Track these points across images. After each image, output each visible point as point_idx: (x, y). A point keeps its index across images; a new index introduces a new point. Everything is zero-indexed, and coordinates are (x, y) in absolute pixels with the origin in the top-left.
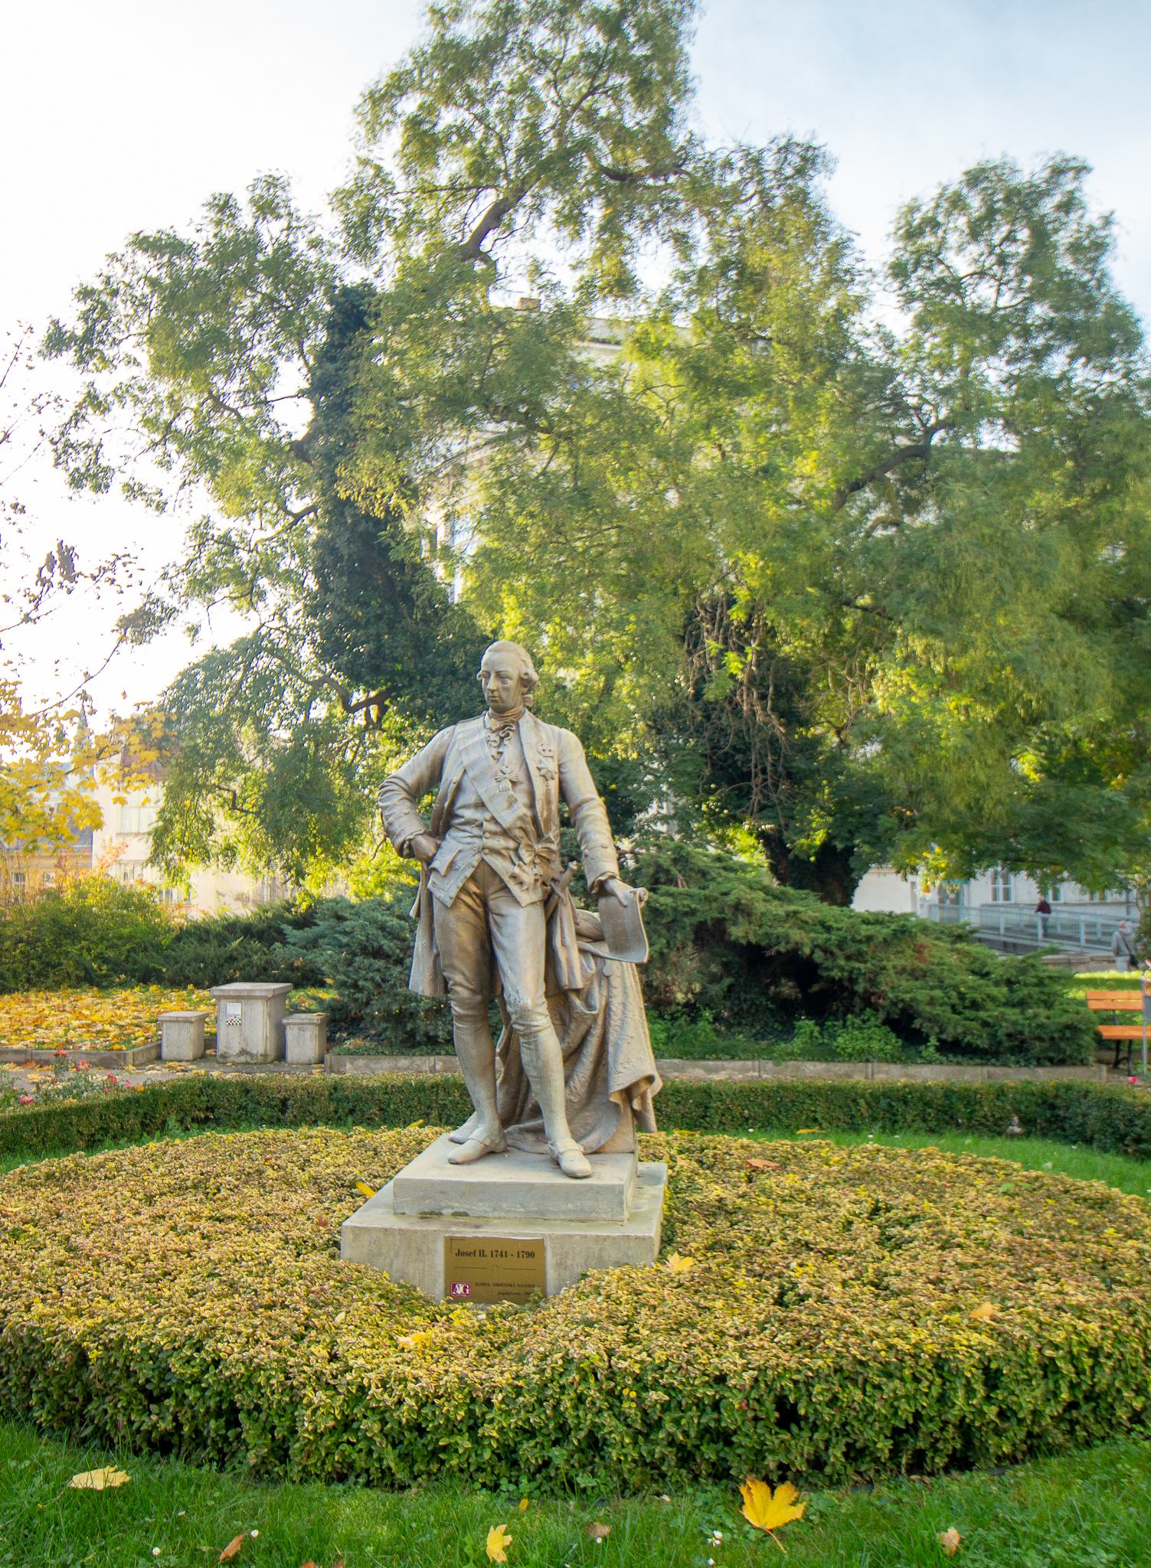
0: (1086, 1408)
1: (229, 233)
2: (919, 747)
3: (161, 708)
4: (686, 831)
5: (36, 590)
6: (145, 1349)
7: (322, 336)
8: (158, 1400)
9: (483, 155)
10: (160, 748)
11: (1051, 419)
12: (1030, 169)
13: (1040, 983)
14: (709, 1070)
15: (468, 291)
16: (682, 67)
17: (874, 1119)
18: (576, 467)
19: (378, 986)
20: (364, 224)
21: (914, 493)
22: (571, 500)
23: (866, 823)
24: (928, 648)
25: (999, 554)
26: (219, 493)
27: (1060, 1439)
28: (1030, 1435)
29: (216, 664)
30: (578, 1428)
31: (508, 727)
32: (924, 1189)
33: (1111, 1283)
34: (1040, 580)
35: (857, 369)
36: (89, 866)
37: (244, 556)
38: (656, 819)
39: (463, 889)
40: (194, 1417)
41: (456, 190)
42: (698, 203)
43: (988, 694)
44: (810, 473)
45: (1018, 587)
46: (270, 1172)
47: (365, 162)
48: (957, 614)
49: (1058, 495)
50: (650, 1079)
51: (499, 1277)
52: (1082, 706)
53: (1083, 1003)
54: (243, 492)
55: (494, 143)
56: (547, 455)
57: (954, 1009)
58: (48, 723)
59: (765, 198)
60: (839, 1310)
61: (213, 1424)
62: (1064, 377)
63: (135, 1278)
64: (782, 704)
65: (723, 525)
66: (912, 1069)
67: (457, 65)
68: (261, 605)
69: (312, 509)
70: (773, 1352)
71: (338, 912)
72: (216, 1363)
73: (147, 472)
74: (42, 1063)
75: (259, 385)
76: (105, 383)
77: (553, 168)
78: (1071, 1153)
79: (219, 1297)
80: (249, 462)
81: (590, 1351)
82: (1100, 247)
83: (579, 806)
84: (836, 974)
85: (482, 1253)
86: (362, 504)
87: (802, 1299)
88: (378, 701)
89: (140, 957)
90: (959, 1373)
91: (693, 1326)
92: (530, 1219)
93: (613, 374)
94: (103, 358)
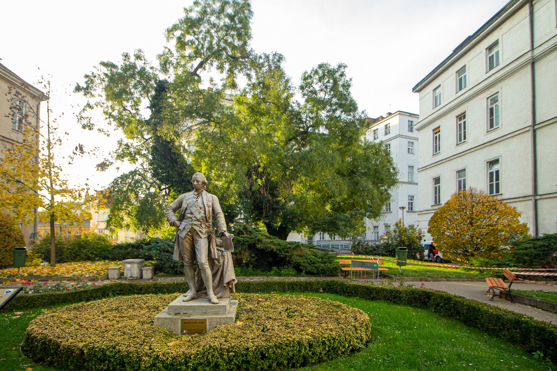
0: (332, 351)
1: (128, 63)
2: (303, 203)
3: (109, 188)
4: (247, 222)
5: (72, 155)
6: (100, 349)
7: (153, 93)
8: (104, 362)
9: (198, 49)
10: (108, 199)
11: (336, 126)
12: (333, 65)
13: (329, 258)
14: (251, 279)
15: (193, 84)
16: (250, 31)
17: (289, 289)
18: (220, 131)
19: (167, 260)
20: (165, 64)
21: (304, 143)
22: (219, 139)
23: (291, 221)
24: (306, 180)
25: (323, 158)
26: (125, 132)
27: (326, 358)
28: (319, 358)
29: (124, 177)
30: (212, 362)
31: (199, 194)
32: (298, 304)
33: (339, 323)
34: (332, 165)
35: (292, 111)
36: (89, 230)
37: (132, 150)
38: (240, 219)
39: (187, 234)
40: (113, 365)
41: (191, 58)
42: (252, 66)
43: (319, 191)
44: (279, 136)
45: (327, 166)
46: (136, 305)
47: (166, 48)
48: (313, 172)
49: (337, 144)
50: (234, 280)
51: (194, 328)
52: (340, 194)
53: (338, 262)
54: (132, 132)
55: (201, 46)
56: (213, 128)
57: (309, 264)
58: (76, 191)
59: (269, 66)
60: (276, 332)
61: (118, 367)
62: (340, 116)
63: (97, 332)
64: (271, 192)
65: (258, 148)
66: (299, 278)
67: (191, 24)
68: (136, 162)
69: (151, 138)
70: (261, 342)
71: (157, 241)
72: (119, 352)
73: (106, 127)
74: (75, 280)
75: (136, 104)
76: (92, 101)
77: (217, 54)
78: (333, 296)
79: (120, 336)
80: (134, 125)
81: (216, 344)
82: (349, 86)
83: (217, 214)
84: (282, 256)
85: (190, 323)
86: (164, 137)
87: (268, 330)
88: (168, 188)
89: (103, 253)
90: (303, 345)
91: (241, 337)
92: (203, 314)
93: (231, 108)
94: (91, 94)
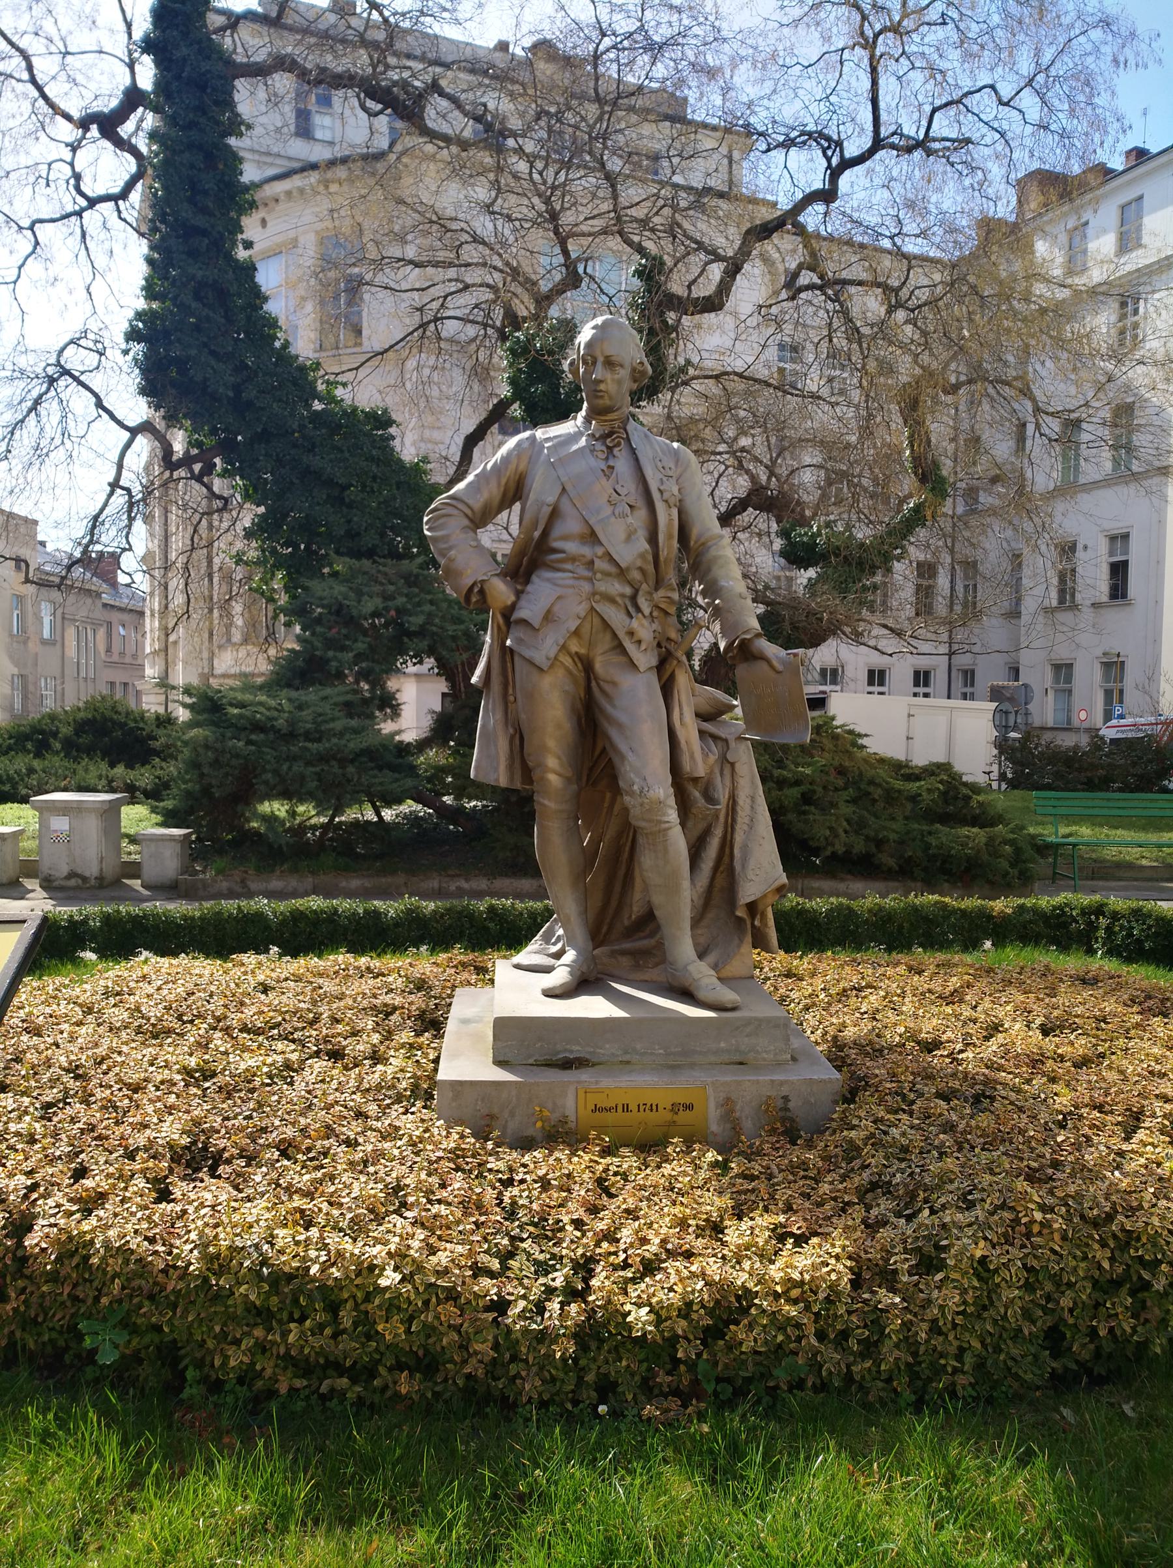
39: (564, 648)
